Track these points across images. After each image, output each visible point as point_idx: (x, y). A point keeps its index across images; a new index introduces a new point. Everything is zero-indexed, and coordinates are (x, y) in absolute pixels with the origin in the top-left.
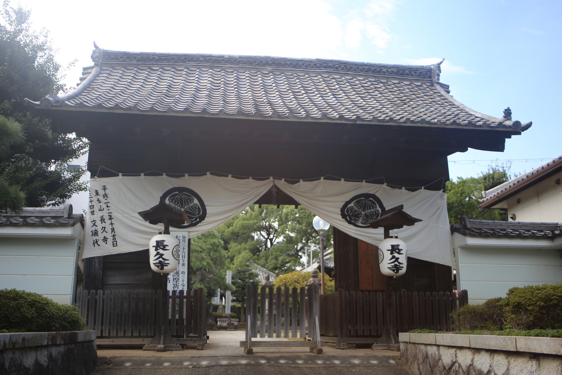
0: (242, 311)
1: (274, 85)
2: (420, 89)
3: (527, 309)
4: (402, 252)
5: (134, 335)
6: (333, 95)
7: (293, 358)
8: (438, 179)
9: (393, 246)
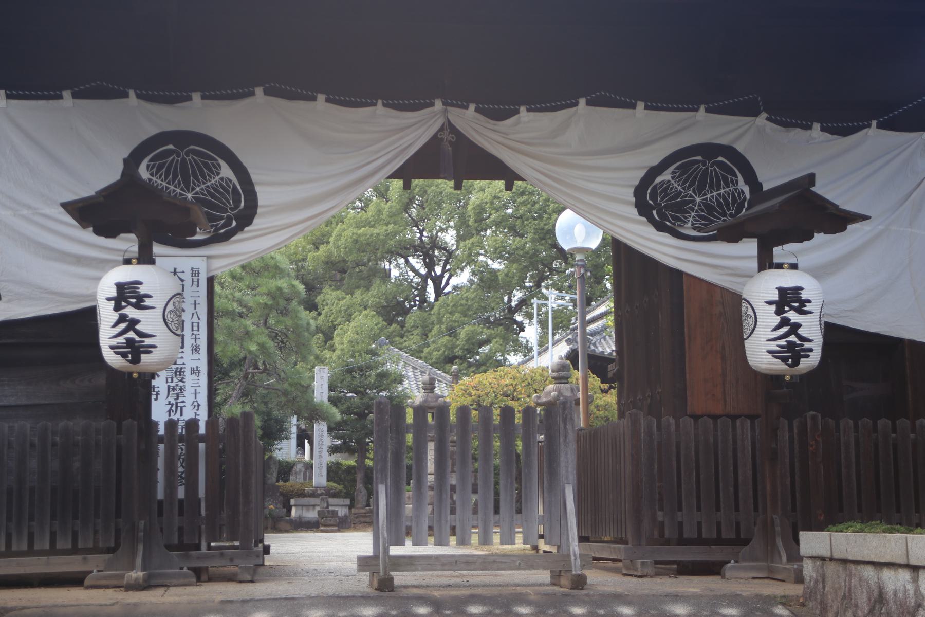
0: (359, 476)
4: (808, 307)
5: (60, 545)
9: (782, 291)
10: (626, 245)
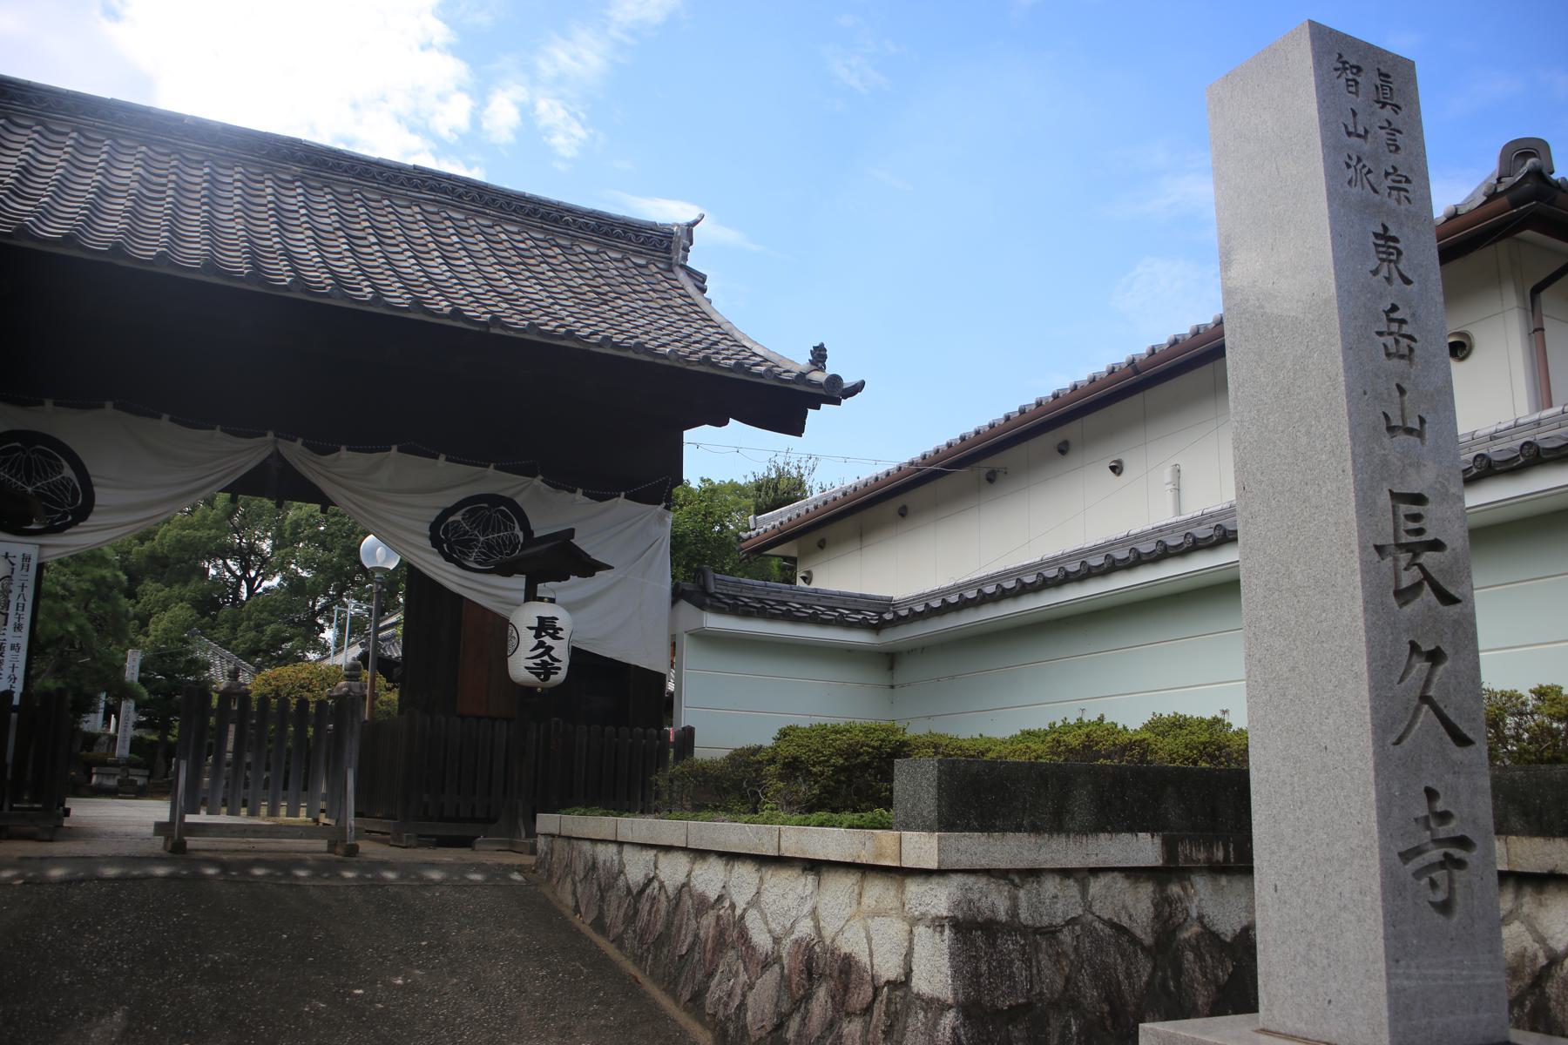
1: (303, 211)
2: (641, 275)
3: (809, 772)
4: (560, 634)
6: (443, 257)
7: (284, 865)
8: (657, 478)
10: (418, 571)
